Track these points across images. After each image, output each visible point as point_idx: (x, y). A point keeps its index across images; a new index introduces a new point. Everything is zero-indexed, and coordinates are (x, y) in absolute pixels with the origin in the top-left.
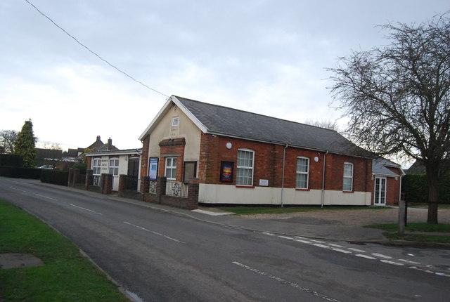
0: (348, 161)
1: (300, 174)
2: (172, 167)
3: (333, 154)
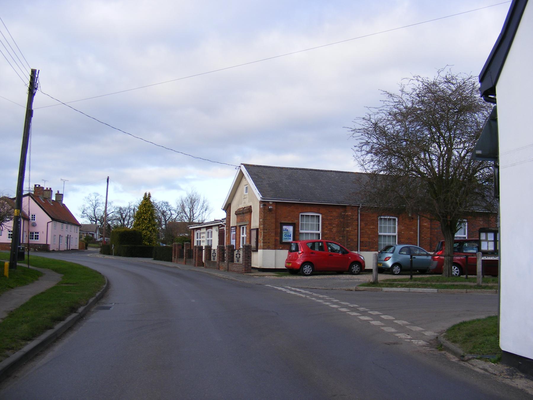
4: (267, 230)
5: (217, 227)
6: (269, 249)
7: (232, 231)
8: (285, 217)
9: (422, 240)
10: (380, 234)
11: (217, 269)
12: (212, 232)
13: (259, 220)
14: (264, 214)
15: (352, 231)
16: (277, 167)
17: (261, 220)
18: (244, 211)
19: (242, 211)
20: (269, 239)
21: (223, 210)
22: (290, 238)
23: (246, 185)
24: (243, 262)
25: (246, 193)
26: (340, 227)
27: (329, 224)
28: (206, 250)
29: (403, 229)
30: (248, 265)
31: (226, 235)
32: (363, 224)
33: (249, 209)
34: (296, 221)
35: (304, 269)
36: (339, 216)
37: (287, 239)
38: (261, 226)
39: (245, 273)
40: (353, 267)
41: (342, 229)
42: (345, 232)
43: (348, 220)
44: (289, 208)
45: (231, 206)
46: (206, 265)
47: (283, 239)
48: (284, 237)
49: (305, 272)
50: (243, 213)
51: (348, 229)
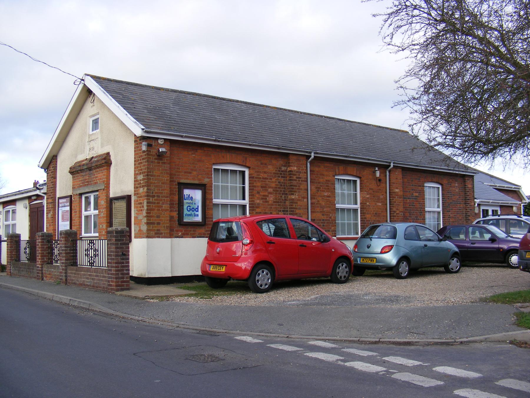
0: (429, 181)
1: (343, 210)
2: (92, 212)
3: (403, 169)
4: (154, 196)
5: (27, 202)
6: (159, 237)
7: (60, 205)
8: (188, 172)
9: (394, 216)
10: (338, 206)
11: (38, 279)
12: (14, 212)
13: (135, 178)
14: (148, 165)
15: (299, 200)
16: (150, 87)
17: (141, 177)
18: (92, 163)
19: (87, 164)
20: (158, 217)
21: (42, 168)
22: (197, 213)
23: (94, 116)
24: (112, 267)
25: (93, 131)
26: (280, 194)
27: (262, 187)
28: (11, 242)
29: (368, 198)
30: (122, 274)
31: (47, 213)
32: (313, 187)
33: (105, 159)
34: (206, 181)
35: (257, 278)
36: (278, 174)
37: (191, 215)
38: (142, 189)
39: (118, 290)
40: (339, 268)
41: (283, 196)
42: (288, 203)
43: (292, 180)
44: (193, 154)
45: (57, 159)
46: (10, 270)
47: (184, 215)
48: (186, 212)
49: (259, 284)
50: (90, 169)
51: (293, 197)
